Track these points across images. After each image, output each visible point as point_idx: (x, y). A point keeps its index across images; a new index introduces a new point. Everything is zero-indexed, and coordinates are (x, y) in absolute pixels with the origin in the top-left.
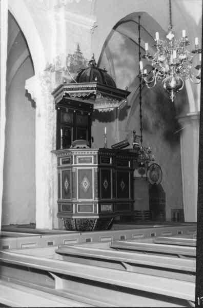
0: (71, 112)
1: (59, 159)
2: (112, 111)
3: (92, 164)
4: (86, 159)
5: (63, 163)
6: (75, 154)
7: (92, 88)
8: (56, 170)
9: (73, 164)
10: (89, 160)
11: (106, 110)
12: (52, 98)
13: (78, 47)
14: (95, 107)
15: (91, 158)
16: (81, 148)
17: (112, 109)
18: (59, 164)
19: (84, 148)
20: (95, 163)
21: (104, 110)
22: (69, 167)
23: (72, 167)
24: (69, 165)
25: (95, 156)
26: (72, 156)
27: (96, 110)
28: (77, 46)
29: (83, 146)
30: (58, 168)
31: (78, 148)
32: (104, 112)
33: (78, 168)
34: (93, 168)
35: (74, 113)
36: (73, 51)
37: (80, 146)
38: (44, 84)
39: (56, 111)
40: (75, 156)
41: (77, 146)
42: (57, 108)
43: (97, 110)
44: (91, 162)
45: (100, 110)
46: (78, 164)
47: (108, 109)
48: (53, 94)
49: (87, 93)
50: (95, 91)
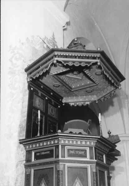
0: (43, 97)
1: (29, 152)
2: (88, 105)
3: (88, 159)
4: (77, 152)
5: (37, 157)
6: (62, 142)
7: (94, 58)
8: (22, 169)
9: (60, 158)
10: (83, 153)
11: (80, 104)
12: (25, 75)
13: (53, 33)
14: (64, 101)
15: (85, 151)
16: (76, 134)
17: (88, 103)
18: (28, 160)
19: (80, 133)
20: (91, 158)
21: (78, 103)
22: (51, 163)
23: (57, 162)
24: (53, 159)
25: (91, 148)
26: (57, 147)
27: (65, 103)
28: (52, 34)
29: (78, 131)
30: (26, 167)
31: (71, 133)
32: (78, 106)
33: (67, 165)
34: (89, 165)
35: (46, 100)
36: (50, 36)
37: (74, 131)
38: (16, 59)
39: (27, 92)
40: (63, 146)
41: (70, 130)
42: (29, 87)
43: (67, 104)
44: (86, 157)
45: (71, 104)
46: (67, 158)
47: (82, 103)
48: (26, 70)
49: (89, 63)
50: (98, 61)
